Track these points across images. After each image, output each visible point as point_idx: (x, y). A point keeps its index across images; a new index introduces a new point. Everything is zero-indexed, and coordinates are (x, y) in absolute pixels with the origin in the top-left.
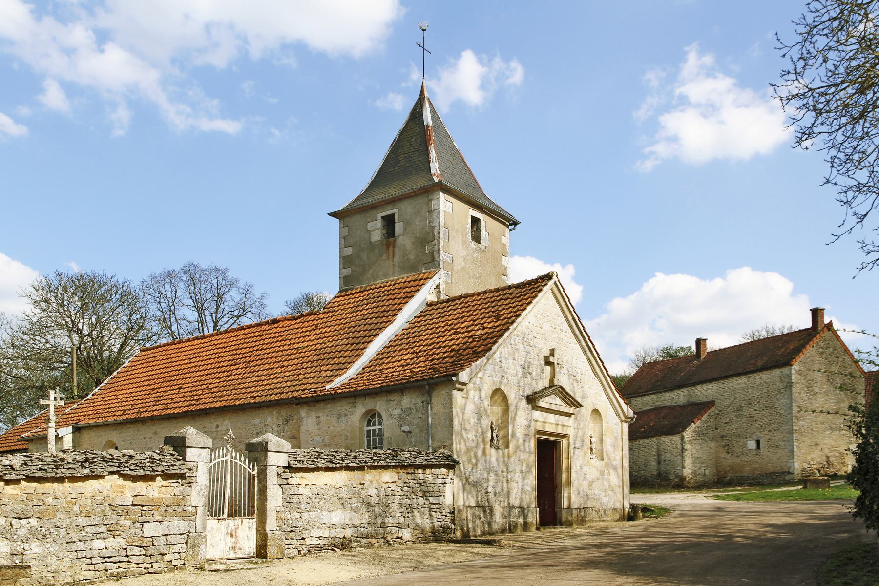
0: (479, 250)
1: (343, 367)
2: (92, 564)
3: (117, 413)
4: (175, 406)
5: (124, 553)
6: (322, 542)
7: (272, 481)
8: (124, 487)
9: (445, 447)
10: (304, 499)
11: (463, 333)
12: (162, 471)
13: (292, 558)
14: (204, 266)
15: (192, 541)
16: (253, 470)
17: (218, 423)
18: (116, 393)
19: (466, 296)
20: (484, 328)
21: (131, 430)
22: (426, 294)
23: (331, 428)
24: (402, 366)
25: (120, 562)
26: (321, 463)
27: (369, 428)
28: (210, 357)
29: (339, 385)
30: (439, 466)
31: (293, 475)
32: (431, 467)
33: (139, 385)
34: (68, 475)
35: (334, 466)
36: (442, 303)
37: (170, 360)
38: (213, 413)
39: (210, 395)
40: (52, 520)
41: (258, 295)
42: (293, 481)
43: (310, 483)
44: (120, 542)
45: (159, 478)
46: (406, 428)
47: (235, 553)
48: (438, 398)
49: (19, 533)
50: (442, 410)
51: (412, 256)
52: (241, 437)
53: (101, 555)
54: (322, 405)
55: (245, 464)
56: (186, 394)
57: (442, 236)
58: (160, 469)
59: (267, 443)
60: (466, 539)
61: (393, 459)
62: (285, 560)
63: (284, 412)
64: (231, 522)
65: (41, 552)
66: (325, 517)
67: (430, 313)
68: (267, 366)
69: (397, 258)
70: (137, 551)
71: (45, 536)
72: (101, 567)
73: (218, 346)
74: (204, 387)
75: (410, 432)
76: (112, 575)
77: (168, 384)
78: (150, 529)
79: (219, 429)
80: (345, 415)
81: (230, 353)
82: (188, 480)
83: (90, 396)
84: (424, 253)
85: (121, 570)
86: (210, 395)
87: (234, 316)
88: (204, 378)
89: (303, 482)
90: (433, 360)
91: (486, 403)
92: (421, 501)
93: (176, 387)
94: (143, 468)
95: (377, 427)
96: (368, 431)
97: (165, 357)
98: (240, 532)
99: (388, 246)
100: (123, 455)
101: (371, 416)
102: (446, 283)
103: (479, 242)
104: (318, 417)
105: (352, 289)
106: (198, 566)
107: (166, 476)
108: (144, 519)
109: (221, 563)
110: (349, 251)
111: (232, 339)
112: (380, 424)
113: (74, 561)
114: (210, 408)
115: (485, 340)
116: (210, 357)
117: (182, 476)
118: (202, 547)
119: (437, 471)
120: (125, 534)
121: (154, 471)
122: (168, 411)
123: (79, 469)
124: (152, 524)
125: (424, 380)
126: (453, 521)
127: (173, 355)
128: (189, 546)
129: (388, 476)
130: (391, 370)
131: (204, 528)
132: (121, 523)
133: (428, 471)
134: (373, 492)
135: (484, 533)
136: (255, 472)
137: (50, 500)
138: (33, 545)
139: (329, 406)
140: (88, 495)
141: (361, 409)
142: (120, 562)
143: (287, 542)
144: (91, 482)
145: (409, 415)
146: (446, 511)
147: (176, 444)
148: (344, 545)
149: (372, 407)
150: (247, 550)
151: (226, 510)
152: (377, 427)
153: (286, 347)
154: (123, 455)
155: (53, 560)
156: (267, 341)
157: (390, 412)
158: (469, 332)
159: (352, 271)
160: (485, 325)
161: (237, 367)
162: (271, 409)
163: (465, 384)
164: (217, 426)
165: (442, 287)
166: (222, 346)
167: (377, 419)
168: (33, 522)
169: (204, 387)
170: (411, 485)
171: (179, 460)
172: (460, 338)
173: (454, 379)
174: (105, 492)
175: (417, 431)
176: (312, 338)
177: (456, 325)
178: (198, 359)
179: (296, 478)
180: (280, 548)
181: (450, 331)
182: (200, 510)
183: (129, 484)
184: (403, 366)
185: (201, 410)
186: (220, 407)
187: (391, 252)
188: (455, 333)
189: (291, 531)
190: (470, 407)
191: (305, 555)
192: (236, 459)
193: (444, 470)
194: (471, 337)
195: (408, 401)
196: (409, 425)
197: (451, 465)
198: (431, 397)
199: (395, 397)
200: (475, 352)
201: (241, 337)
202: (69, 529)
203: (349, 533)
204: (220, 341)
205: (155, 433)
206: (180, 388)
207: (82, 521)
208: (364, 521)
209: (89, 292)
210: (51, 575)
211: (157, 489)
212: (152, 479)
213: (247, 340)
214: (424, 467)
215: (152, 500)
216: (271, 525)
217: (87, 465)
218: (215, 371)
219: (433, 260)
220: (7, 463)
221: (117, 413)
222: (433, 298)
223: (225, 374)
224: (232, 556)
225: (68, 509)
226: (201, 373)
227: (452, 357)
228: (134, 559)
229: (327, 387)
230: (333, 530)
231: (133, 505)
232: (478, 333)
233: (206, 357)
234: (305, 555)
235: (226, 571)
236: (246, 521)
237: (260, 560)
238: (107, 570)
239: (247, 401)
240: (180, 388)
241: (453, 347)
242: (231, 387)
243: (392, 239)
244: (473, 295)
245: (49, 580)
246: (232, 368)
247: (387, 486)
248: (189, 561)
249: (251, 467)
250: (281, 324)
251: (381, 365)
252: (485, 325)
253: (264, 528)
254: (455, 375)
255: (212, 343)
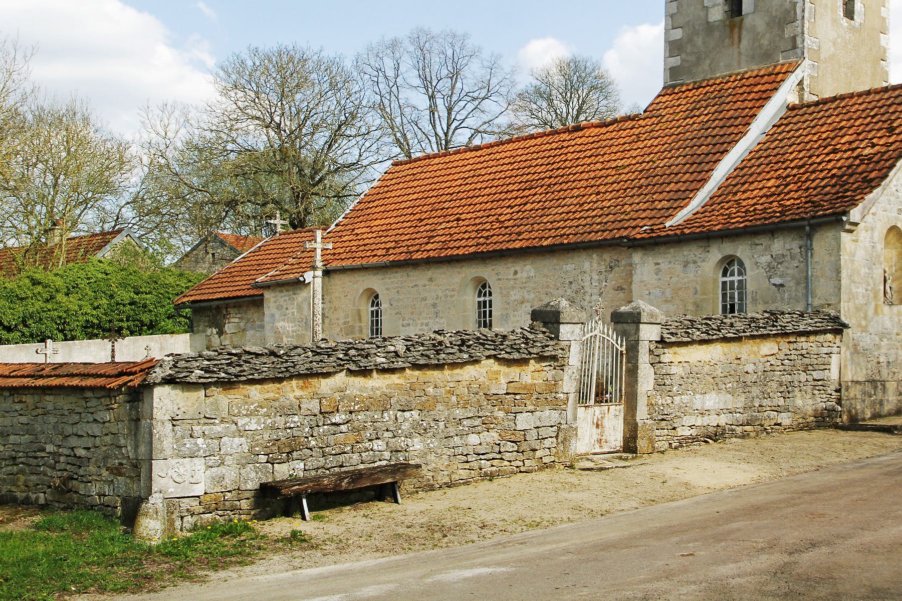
0: (852, 29)
1: (683, 197)
2: (467, 462)
3: (379, 253)
4: (457, 244)
5: (497, 449)
6: (694, 432)
7: (644, 358)
8: (498, 373)
9: (829, 305)
10: (676, 380)
11: (845, 151)
12: (537, 354)
13: (662, 452)
14: (436, 31)
15: (564, 434)
16: (621, 346)
17: (518, 268)
18: (368, 224)
19: (842, 98)
20: (873, 146)
21: (398, 275)
22: (786, 94)
23: (674, 279)
24: (764, 196)
25: (493, 459)
26: (697, 335)
27: (725, 279)
28: (492, 176)
29: (681, 222)
30: (825, 332)
31: (666, 350)
32: (815, 333)
33: (399, 212)
34: (449, 361)
35: (711, 337)
36: (809, 106)
37: (436, 180)
38: (510, 256)
39: (503, 231)
40: (432, 413)
41: (507, 69)
42: (664, 359)
43: (683, 360)
44: (493, 436)
45: (532, 361)
46: (777, 281)
47: (601, 447)
48: (821, 242)
49: (403, 427)
50: (827, 258)
51: (765, 42)
52: (548, 287)
53: (476, 451)
54: (662, 249)
55: (612, 338)
56: (470, 229)
57: (806, 15)
58: (535, 350)
59: (639, 314)
60: (854, 425)
61: (773, 326)
62: (655, 455)
63: (607, 256)
64: (597, 410)
65: (422, 448)
66: (698, 402)
67: (795, 120)
68: (576, 192)
69: (745, 43)
70: (510, 446)
71: (425, 430)
72: (475, 465)
73: (501, 162)
74: (491, 219)
75: (782, 285)
76: (486, 474)
77: (439, 213)
78: (524, 421)
79: (518, 276)
80: (695, 262)
81: (520, 172)
82: (561, 362)
83: (333, 226)
84: (781, 36)
85: (494, 469)
86: (503, 231)
87: (474, 99)
88: (489, 206)
89: (676, 359)
90: (807, 189)
91: (880, 246)
92: (803, 377)
93: (452, 218)
94: (518, 350)
95: (736, 278)
96: (724, 283)
97: (428, 175)
98: (606, 423)
99: (732, 27)
100: (496, 335)
101: (728, 263)
102: (812, 77)
103: (852, 19)
104: (658, 264)
105: (682, 85)
106: (568, 464)
107: (541, 358)
108: (517, 409)
109: (588, 459)
110: (678, 34)
111: (520, 152)
112: (740, 274)
113: (452, 458)
114: (508, 249)
115: (877, 162)
116: (492, 176)
117: (554, 358)
118: (573, 441)
119: (821, 338)
120: (499, 427)
121: (530, 353)
122: (450, 252)
123: (458, 354)
124: (525, 414)
125: (803, 219)
126: (839, 401)
127: (439, 173)
128: (559, 440)
129: (768, 347)
130: (751, 202)
131: (575, 419)
132: (495, 414)
133: (812, 338)
134: (750, 368)
135: (876, 416)
136: (624, 349)
137: (430, 390)
138: (416, 440)
139: (672, 251)
140: (464, 383)
141: (716, 253)
142: (493, 459)
143: (658, 432)
144: (469, 368)
145: (781, 263)
146: (831, 389)
147: (547, 320)
148: (716, 435)
149: (731, 253)
150: (614, 443)
151: (593, 396)
152: (736, 278)
153: (599, 166)
154: (496, 335)
155: (432, 457)
156: (570, 156)
157: (755, 257)
158: (853, 150)
159: (683, 60)
160: (875, 141)
161: (533, 191)
162: (590, 252)
163: (856, 224)
164: (516, 273)
165: (806, 83)
166: (507, 161)
167: (736, 268)
168: (415, 413)
169: (491, 219)
170: (792, 357)
171: (551, 339)
172: (840, 161)
173: (844, 218)
174: (482, 379)
175: (792, 284)
176: (635, 153)
177: (833, 139)
178: (475, 179)
179: (668, 355)
180: (651, 441)
181: (825, 147)
182: (572, 397)
183: (504, 369)
184: (767, 197)
185: (494, 251)
186: (521, 248)
187: (736, 36)
188: (835, 151)
189: (663, 420)
190: (860, 254)
191: (676, 448)
192: (604, 333)
193: (829, 336)
194: (856, 158)
195: (779, 245)
196: (781, 276)
197: (838, 328)
198: (811, 241)
199: (764, 241)
200: (864, 180)
201: (533, 149)
202: (447, 421)
203: (723, 420)
204: (503, 155)
205: (431, 280)
206: (458, 220)
207: (459, 413)
208: (740, 405)
209: (287, 74)
210: (431, 474)
211: (532, 374)
212: (523, 362)
213: (541, 154)
214: (806, 334)
215: (525, 387)
216: (642, 413)
217: (464, 348)
218: (503, 196)
219: (795, 47)
220: (392, 349)
221: (379, 253)
222: (794, 99)
223: (518, 201)
224: (598, 450)
225: (446, 400)
226: (485, 199)
227: (834, 186)
228: (507, 456)
229: (668, 224)
230: (706, 417)
231: (507, 394)
232: (866, 152)
233: (487, 177)
234: (676, 448)
235: (601, 469)
236: (612, 408)
237: (630, 456)
238: (481, 469)
239: (558, 241)
240: (458, 220)
241: (834, 171)
242: (531, 221)
243: (737, 19)
244: (852, 96)
245: (429, 480)
246: (527, 193)
247: (766, 359)
248: (559, 458)
249: (619, 342)
250: (587, 132)
251: (735, 194)
252: (875, 141)
253: (634, 416)
254: (845, 213)
255: (493, 157)
